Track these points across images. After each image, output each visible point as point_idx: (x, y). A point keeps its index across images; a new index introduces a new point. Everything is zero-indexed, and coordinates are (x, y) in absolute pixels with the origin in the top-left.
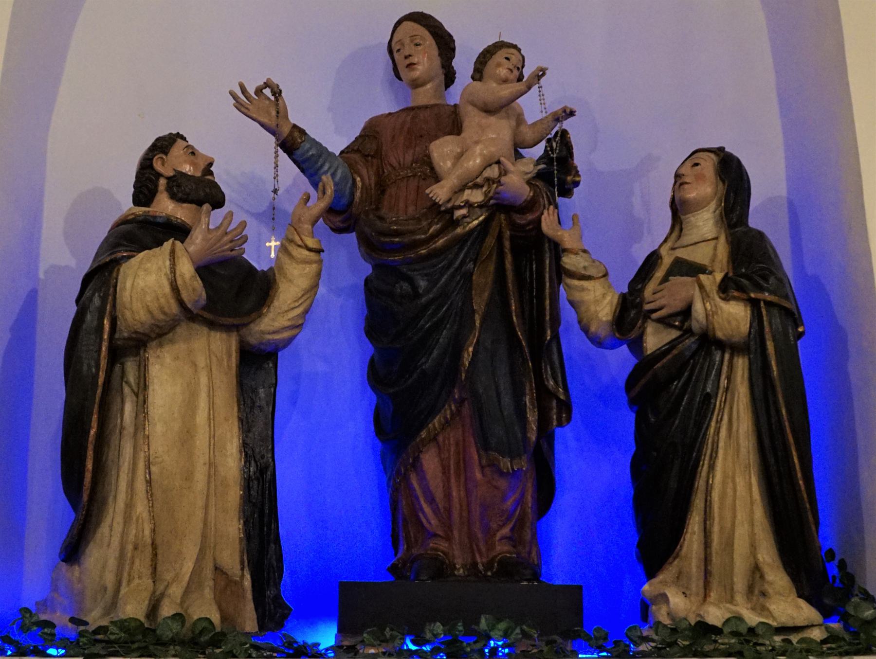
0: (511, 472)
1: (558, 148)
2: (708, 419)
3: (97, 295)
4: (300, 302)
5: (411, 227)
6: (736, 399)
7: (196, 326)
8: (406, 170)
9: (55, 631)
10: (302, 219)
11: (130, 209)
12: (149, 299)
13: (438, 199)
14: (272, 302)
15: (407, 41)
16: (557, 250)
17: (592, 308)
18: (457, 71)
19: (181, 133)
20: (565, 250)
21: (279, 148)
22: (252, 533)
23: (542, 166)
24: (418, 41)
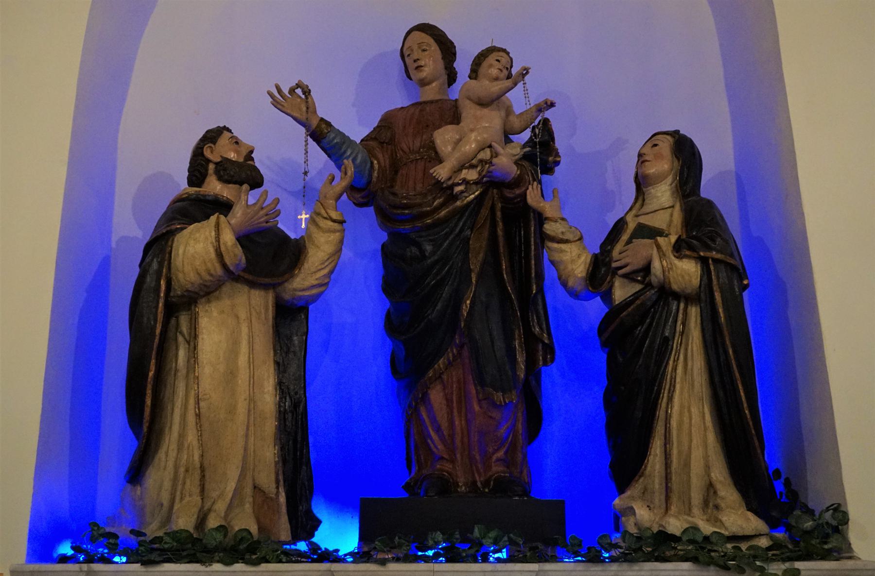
0: (503, 404)
1: (540, 134)
2: (667, 359)
3: (155, 260)
4: (326, 264)
5: (418, 201)
6: (690, 341)
8: (415, 154)
9: (118, 542)
10: (328, 195)
11: (185, 190)
12: (198, 264)
13: (440, 177)
14: (303, 264)
15: (415, 47)
16: (541, 219)
17: (570, 267)
18: (458, 71)
19: (227, 126)
20: (547, 219)
21: (309, 137)
22: (287, 457)
23: (528, 149)
24: (424, 47)
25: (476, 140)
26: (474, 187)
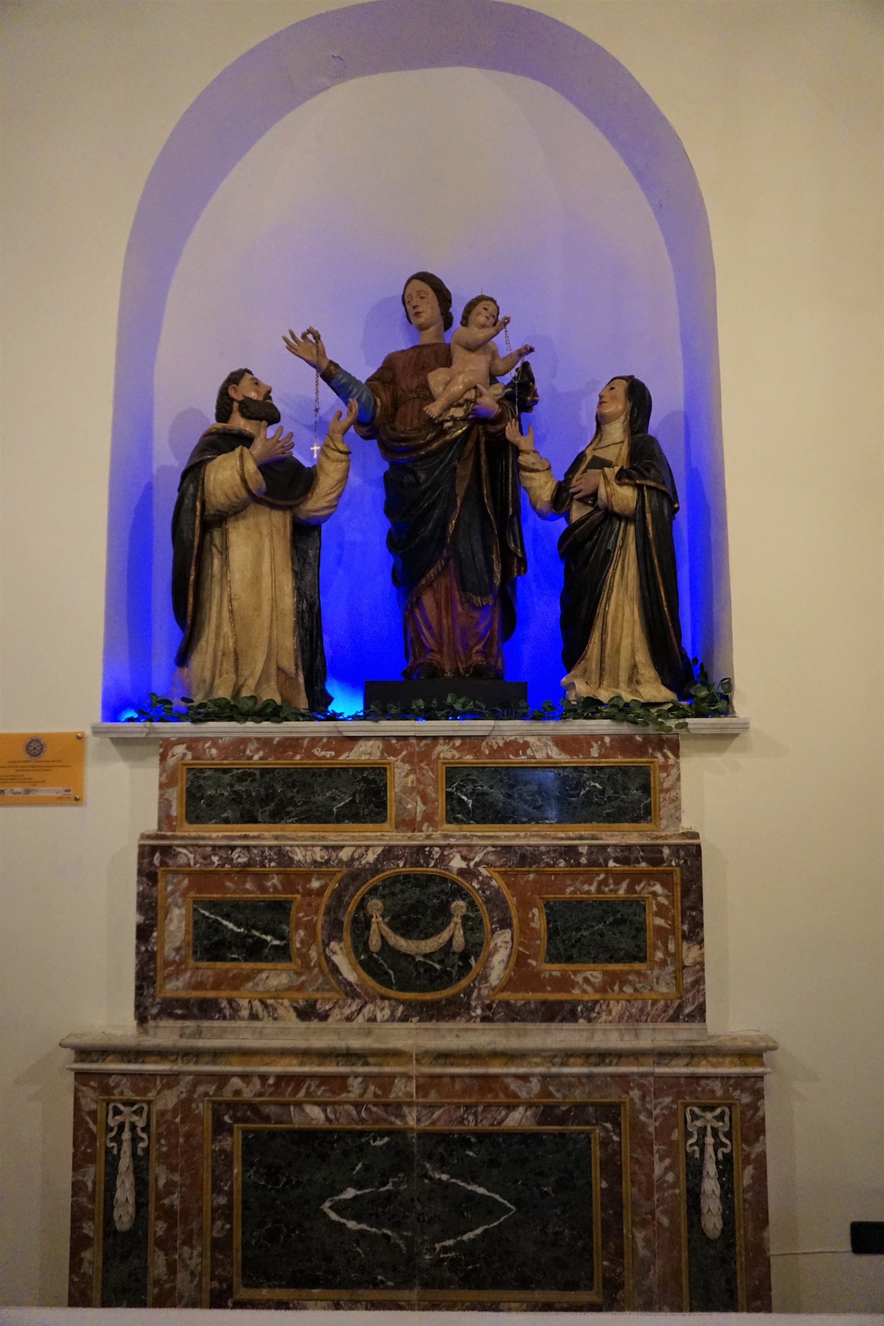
7: (262, 507)
14: (315, 489)
15: (414, 295)
16: (517, 451)
17: (538, 492)
23: (509, 390)
24: (423, 295)
25: (463, 382)
26: (462, 423)
